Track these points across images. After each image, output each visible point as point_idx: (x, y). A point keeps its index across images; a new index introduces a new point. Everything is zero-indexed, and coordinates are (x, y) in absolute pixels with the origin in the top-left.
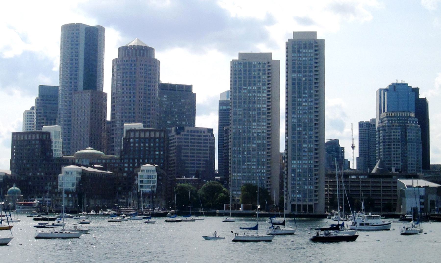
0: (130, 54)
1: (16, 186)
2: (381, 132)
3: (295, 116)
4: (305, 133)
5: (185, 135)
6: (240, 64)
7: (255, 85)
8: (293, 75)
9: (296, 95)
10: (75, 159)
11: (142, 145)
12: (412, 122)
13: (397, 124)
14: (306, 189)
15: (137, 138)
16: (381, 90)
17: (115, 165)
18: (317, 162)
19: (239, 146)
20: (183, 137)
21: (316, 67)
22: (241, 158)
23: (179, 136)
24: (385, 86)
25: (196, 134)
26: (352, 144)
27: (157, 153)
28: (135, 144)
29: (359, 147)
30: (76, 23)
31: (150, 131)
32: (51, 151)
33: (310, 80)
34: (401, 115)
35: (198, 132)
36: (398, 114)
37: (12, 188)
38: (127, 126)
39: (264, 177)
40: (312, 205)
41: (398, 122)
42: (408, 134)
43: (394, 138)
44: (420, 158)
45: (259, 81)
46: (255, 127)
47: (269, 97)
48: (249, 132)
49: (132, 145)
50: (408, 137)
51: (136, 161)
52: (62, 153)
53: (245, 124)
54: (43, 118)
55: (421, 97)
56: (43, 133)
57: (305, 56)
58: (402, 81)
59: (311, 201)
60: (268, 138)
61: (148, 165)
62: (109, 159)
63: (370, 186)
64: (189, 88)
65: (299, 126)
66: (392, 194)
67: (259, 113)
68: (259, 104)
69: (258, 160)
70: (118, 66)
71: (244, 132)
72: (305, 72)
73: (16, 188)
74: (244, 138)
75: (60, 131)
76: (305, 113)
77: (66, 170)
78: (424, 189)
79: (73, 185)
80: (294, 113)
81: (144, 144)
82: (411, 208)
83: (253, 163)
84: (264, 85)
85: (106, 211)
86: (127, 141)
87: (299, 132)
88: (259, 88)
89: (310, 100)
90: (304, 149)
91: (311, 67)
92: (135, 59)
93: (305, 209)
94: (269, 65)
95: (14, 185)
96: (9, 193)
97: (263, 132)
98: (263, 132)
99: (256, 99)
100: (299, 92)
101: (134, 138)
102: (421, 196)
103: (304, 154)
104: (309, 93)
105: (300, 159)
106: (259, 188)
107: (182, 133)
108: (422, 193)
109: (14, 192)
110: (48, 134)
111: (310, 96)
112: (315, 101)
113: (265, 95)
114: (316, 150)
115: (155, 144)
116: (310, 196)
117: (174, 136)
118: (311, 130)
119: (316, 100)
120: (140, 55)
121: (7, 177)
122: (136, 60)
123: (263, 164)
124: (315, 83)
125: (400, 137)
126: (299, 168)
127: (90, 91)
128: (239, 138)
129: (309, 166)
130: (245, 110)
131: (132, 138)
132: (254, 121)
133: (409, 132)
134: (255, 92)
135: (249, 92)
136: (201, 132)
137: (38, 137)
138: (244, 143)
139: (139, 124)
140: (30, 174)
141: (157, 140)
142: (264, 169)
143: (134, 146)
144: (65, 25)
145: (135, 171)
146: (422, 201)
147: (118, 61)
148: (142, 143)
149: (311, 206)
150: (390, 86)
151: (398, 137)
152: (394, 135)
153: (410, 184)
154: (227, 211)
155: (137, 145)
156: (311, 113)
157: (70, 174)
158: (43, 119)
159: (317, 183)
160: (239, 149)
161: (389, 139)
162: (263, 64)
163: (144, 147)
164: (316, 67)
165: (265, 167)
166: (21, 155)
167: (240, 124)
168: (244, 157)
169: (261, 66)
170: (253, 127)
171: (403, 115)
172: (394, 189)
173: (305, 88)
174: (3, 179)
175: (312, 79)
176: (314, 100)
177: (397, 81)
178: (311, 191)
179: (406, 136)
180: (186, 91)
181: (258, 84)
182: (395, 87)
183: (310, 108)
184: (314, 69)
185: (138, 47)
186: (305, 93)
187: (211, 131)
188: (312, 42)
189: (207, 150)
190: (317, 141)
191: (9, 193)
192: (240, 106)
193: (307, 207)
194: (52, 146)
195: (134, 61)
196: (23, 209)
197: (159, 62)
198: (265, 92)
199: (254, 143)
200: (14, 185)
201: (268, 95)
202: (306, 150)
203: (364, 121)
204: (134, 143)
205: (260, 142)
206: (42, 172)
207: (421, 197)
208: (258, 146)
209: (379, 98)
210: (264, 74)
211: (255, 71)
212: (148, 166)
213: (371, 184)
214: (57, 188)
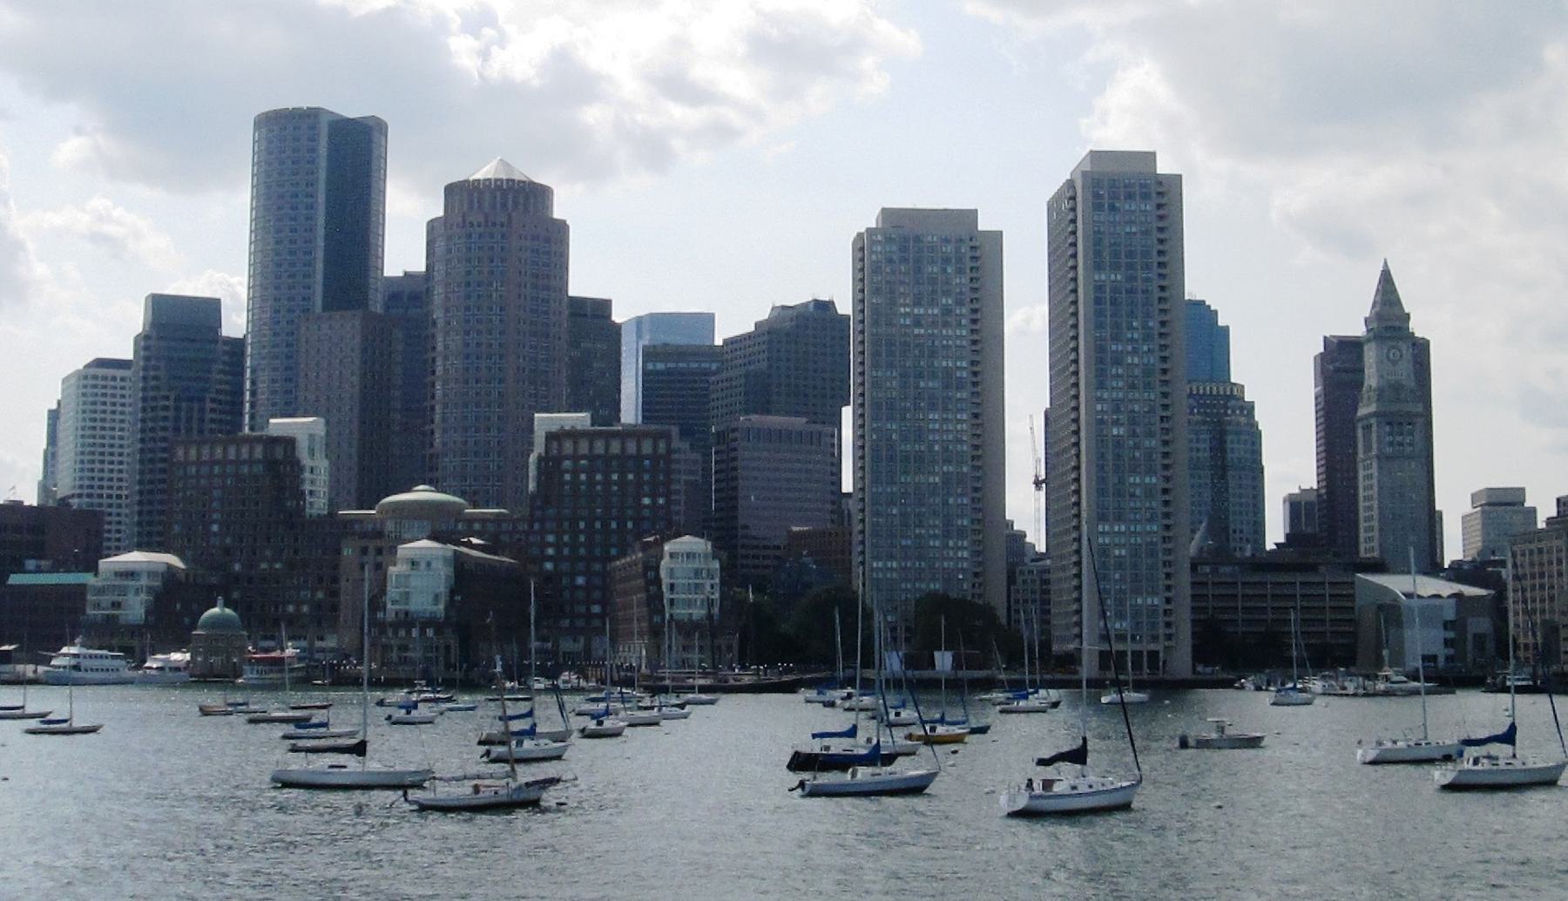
0: (486, 204)
1: (226, 605)
3: (1106, 396)
4: (1135, 444)
6: (889, 240)
7: (933, 303)
9: (1107, 333)
10: (383, 522)
12: (1238, 412)
13: (1199, 418)
14: (1141, 606)
15: (584, 457)
17: (531, 538)
18: (1167, 527)
19: (892, 482)
22: (895, 515)
26: (1034, 474)
27: (646, 501)
28: (626, 476)
30: (308, 108)
33: (1145, 291)
34: (1215, 393)
36: (1201, 388)
37: (216, 610)
38: (545, 421)
39: (963, 570)
40: (1158, 652)
41: (1202, 410)
42: (1229, 446)
45: (946, 293)
46: (937, 426)
48: (919, 438)
49: (567, 477)
50: (1229, 455)
51: (582, 525)
53: (908, 416)
54: (167, 393)
56: (274, 441)
57: (1131, 222)
59: (1155, 638)
60: (973, 458)
61: (687, 538)
62: (493, 522)
63: (1236, 596)
64: (832, 303)
65: (1116, 423)
67: (947, 387)
68: (947, 357)
69: (948, 523)
70: (449, 238)
71: (904, 439)
72: (1130, 266)
73: (227, 611)
74: (906, 459)
76: (1133, 387)
77: (410, 554)
78: (1453, 601)
80: (1101, 386)
81: (607, 475)
83: (932, 532)
84: (960, 303)
85: (556, 677)
86: (549, 465)
87: (1118, 442)
88: (947, 311)
89: (1145, 348)
90: (1132, 490)
91: (1146, 254)
92: (504, 220)
93: (1137, 665)
94: (972, 244)
95: (220, 600)
96: (204, 627)
97: (960, 441)
98: (960, 441)
99: (936, 344)
100: (1117, 326)
101: (575, 458)
103: (1132, 505)
104: (1143, 328)
105: (1119, 518)
109: (217, 623)
110: (289, 443)
111: (1147, 338)
112: (1162, 351)
113: (964, 333)
114: (1165, 491)
115: (638, 475)
116: (1154, 625)
118: (1151, 435)
119: (1164, 347)
121: (174, 575)
122: (483, 223)
123: (961, 532)
124: (1160, 299)
125: (1207, 454)
126: (1119, 546)
128: (891, 458)
129: (1149, 540)
130: (904, 375)
132: (933, 407)
133: (1232, 442)
134: (934, 324)
138: (906, 473)
139: (311, 419)
140: (237, 567)
142: (963, 548)
143: (575, 482)
144: (269, 112)
146: (1451, 635)
147: (452, 225)
149: (1153, 655)
153: (1409, 588)
155: (583, 477)
157: (423, 566)
159: (1168, 588)
162: (957, 242)
163: (607, 483)
165: (965, 543)
166: (241, 507)
167: (891, 419)
168: (903, 515)
169: (949, 248)
170: (931, 426)
171: (1201, 392)
173: (1132, 314)
174: (164, 584)
175: (1150, 288)
176: (1157, 348)
178: (1153, 610)
179: (1224, 451)
180: (595, 316)
181: (944, 301)
183: (1148, 371)
184: (1155, 259)
185: (499, 183)
186: (1131, 328)
190: (1166, 467)
191: (204, 627)
192: (891, 365)
193: (1145, 659)
194: (303, 481)
196: (267, 676)
198: (964, 322)
199: (933, 473)
200: (220, 600)
201: (973, 331)
202: (1138, 492)
205: (951, 469)
206: (276, 561)
207: (1447, 625)
208: (947, 479)
210: (960, 271)
211: (933, 262)
212: (688, 542)
213: (1269, 590)
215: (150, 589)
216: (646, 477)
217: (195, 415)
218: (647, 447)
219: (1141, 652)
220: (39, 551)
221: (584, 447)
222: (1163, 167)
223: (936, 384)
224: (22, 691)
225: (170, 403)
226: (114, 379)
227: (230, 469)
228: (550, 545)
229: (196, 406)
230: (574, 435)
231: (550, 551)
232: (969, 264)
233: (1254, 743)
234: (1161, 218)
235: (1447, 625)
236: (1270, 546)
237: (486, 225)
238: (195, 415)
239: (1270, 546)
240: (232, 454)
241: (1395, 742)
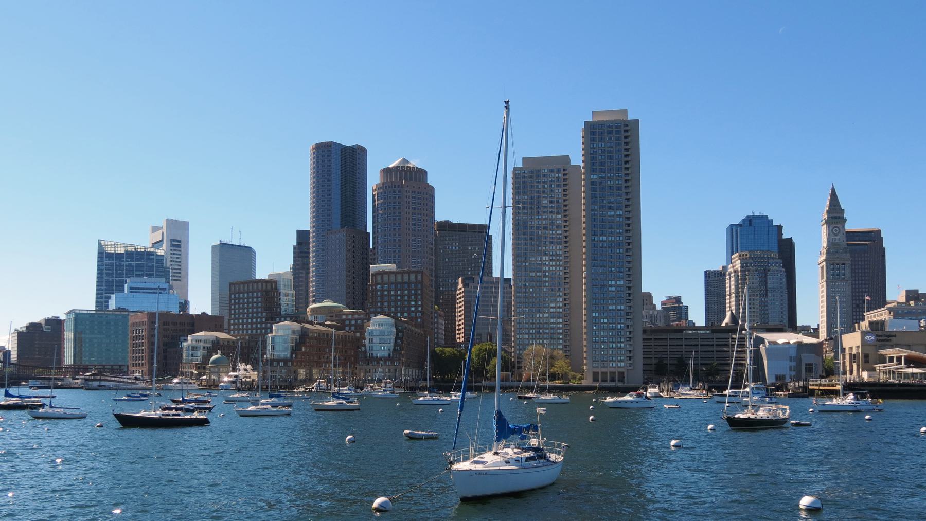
2: (732, 275)
8: (592, 177)
11: (399, 292)
16: (732, 226)
21: (626, 162)
24: (737, 221)
29: (705, 299)
32: (279, 305)
40: (623, 373)
44: (786, 313)
47: (566, 219)
52: (294, 309)
55: (785, 236)
58: (760, 213)
75: (290, 278)
79: (285, 350)
82: (180, 241)
102: (790, 357)
108: (793, 353)
120: (406, 179)
145: (365, 325)
148: (398, 290)
150: (743, 220)
154: (542, 383)
155: (392, 293)
160: (520, 295)
163: (396, 295)
164: (626, 162)
177: (753, 213)
182: (750, 220)
188: (619, 125)
197: (433, 188)
200: (219, 352)
202: (547, 274)
203: (712, 270)
204: (382, 290)
209: (729, 237)
216: (413, 292)
218: (413, 277)
219: (598, 372)
221: (386, 278)
222: (630, 117)
224: (18, 389)
232: (563, 183)
235: (791, 359)
236: (461, 278)
237: (392, 187)
239: (461, 278)
241: (159, 394)
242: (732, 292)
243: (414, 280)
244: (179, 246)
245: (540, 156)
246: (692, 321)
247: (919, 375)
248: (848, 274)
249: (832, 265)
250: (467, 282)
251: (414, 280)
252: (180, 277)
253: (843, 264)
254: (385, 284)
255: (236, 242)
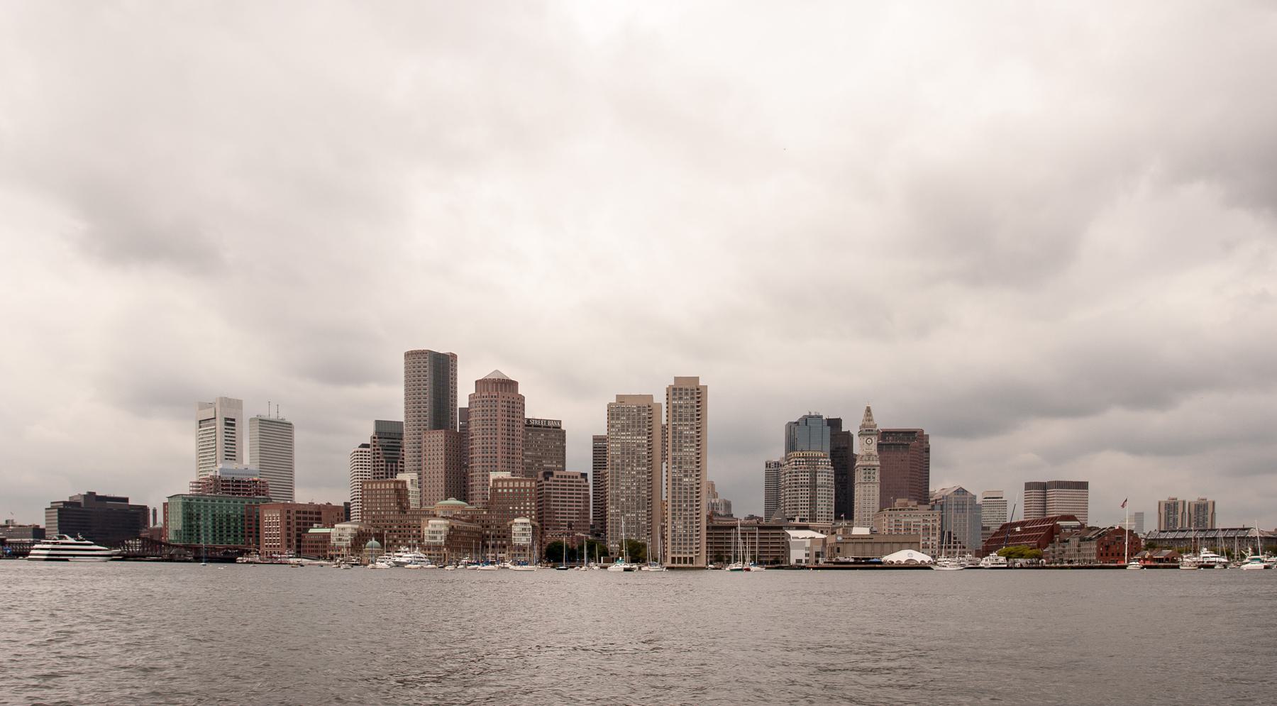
5: (555, 481)
20: (552, 483)
23: (547, 482)
25: (559, 479)
31: (514, 481)
35: (569, 477)
43: (801, 483)
58: (815, 413)
66: (231, 488)
82: (234, 420)
92: (496, 395)
106: (567, 546)
107: (550, 478)
117: (541, 481)
127: (443, 431)
131: (500, 488)
135: (638, 446)
136: (573, 477)
137: (392, 487)
141: (528, 490)
151: (806, 481)
152: (801, 479)
156: (692, 420)
158: (382, 461)
161: (796, 483)
172: (299, 521)
174: (358, 531)
179: (816, 479)
187: (584, 475)
189: (580, 502)
195: (495, 397)
200: (373, 539)
214: (424, 541)
215: (351, 534)
217: (394, 468)
220: (319, 520)
223: (645, 469)
225: (384, 463)
226: (366, 452)
227: (370, 492)
228: (528, 506)
229: (394, 464)
230: (503, 480)
231: (528, 508)
233: (868, 410)
234: (698, 437)
238: (394, 468)
240: (379, 485)
242: (819, 481)
243: (518, 486)
244: (233, 425)
245: (638, 394)
246: (95, 493)
247: (499, 464)
248: (877, 479)
249: (865, 469)
250: (547, 476)
251: (518, 486)
252: (234, 456)
253: (874, 469)
254: (505, 488)
255: (273, 417)
